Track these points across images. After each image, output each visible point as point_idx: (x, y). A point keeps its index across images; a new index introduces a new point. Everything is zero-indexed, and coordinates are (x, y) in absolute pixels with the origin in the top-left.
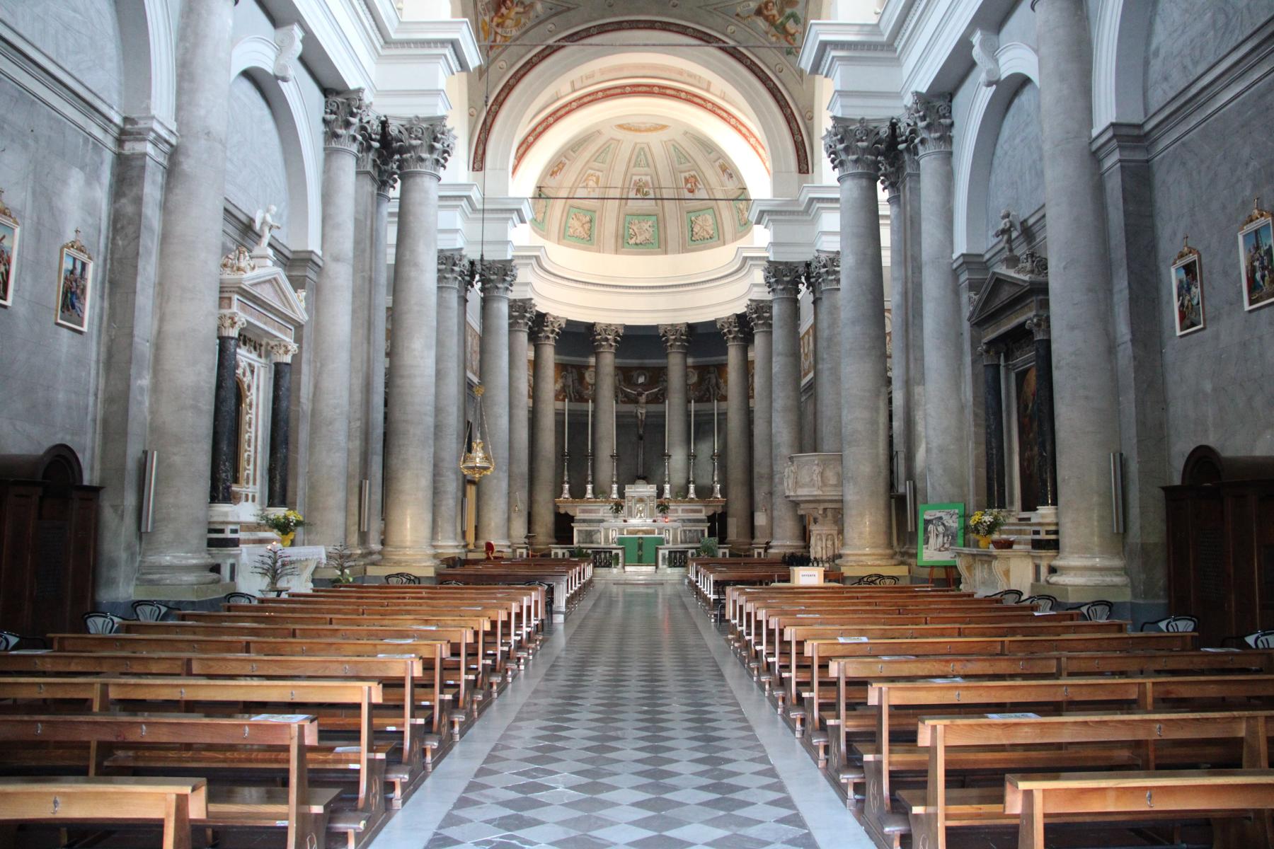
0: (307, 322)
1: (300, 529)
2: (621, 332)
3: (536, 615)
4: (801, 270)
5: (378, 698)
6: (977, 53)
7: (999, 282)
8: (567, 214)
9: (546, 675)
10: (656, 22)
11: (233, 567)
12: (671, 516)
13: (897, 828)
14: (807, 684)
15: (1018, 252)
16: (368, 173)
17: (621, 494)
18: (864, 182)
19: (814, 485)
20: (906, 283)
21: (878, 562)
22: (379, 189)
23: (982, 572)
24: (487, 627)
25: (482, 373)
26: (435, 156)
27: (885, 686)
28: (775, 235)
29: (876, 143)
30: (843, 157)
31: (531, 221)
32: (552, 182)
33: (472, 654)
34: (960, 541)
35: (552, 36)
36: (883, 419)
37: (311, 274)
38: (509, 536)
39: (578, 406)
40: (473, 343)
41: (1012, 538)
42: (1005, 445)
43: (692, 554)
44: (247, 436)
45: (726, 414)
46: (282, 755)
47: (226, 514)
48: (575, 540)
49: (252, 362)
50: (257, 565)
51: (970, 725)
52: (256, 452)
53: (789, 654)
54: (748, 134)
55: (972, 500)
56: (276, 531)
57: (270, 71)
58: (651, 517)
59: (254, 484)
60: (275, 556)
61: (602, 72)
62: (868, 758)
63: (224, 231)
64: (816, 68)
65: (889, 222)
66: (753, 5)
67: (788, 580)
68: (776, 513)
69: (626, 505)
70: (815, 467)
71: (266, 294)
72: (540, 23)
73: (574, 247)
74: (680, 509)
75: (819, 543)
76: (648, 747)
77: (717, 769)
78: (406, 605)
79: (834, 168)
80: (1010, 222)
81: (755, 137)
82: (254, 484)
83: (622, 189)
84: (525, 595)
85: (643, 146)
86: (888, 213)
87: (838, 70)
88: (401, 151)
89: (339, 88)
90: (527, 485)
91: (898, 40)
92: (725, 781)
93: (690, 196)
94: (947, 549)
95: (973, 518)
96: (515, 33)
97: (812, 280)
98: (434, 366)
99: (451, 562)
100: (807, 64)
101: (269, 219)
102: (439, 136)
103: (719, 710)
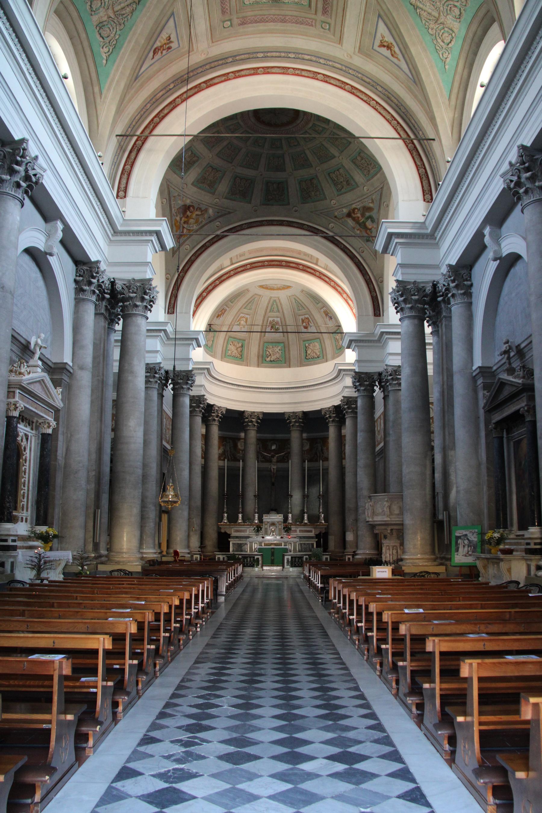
0: (62, 408)
1: (55, 540)
2: (261, 416)
3: (207, 596)
4: (376, 377)
5: (109, 645)
6: (487, 240)
7: (503, 384)
8: (227, 341)
9: (214, 634)
10: (284, 221)
11: (12, 564)
12: (293, 534)
13: (446, 732)
14: (384, 640)
15: (514, 365)
16: (102, 314)
17: (261, 520)
18: (416, 321)
19: (384, 515)
20: (443, 385)
21: (426, 564)
22: (109, 324)
23: (493, 570)
24: (177, 602)
25: (173, 441)
26: (145, 304)
27: (437, 639)
28: (359, 355)
29: (424, 296)
30: (403, 305)
31: (204, 346)
32: (218, 321)
33: (168, 621)
34: (479, 550)
35: (218, 230)
36: (428, 472)
37: (65, 378)
38: (188, 547)
39: (233, 464)
40: (167, 423)
41: (512, 547)
42: (507, 488)
43: (306, 559)
44: (23, 480)
45: (327, 469)
46: (46, 683)
47: (9, 530)
48: (231, 549)
49: (27, 433)
50: (28, 562)
51: (494, 663)
52: (28, 490)
53: (372, 621)
54: (341, 292)
55: (486, 523)
56: (40, 541)
57: (42, 250)
58: (279, 535)
59: (27, 511)
60: (39, 557)
61: (250, 252)
62: (426, 686)
63: (11, 350)
64: (385, 249)
65: (432, 347)
66: (345, 211)
67: (369, 575)
68: (360, 533)
69: (264, 527)
70: (385, 503)
71: (37, 389)
72: (210, 222)
73: (231, 363)
74: (298, 530)
75: (388, 551)
76: (281, 680)
77: (326, 695)
78: (124, 588)
79: (397, 313)
80: (509, 346)
81: (346, 293)
82: (27, 511)
83: (262, 326)
84: (201, 583)
85: (275, 299)
86: (431, 341)
87: (399, 252)
88: (124, 300)
89: (85, 260)
90: (200, 514)
91: (437, 232)
92: (332, 702)
93: (305, 330)
94: (470, 555)
95: (487, 535)
96: (195, 227)
97: (383, 384)
98: (142, 437)
99: (152, 563)
100: (380, 247)
101: (39, 342)
102: (148, 291)
103: (327, 657)
